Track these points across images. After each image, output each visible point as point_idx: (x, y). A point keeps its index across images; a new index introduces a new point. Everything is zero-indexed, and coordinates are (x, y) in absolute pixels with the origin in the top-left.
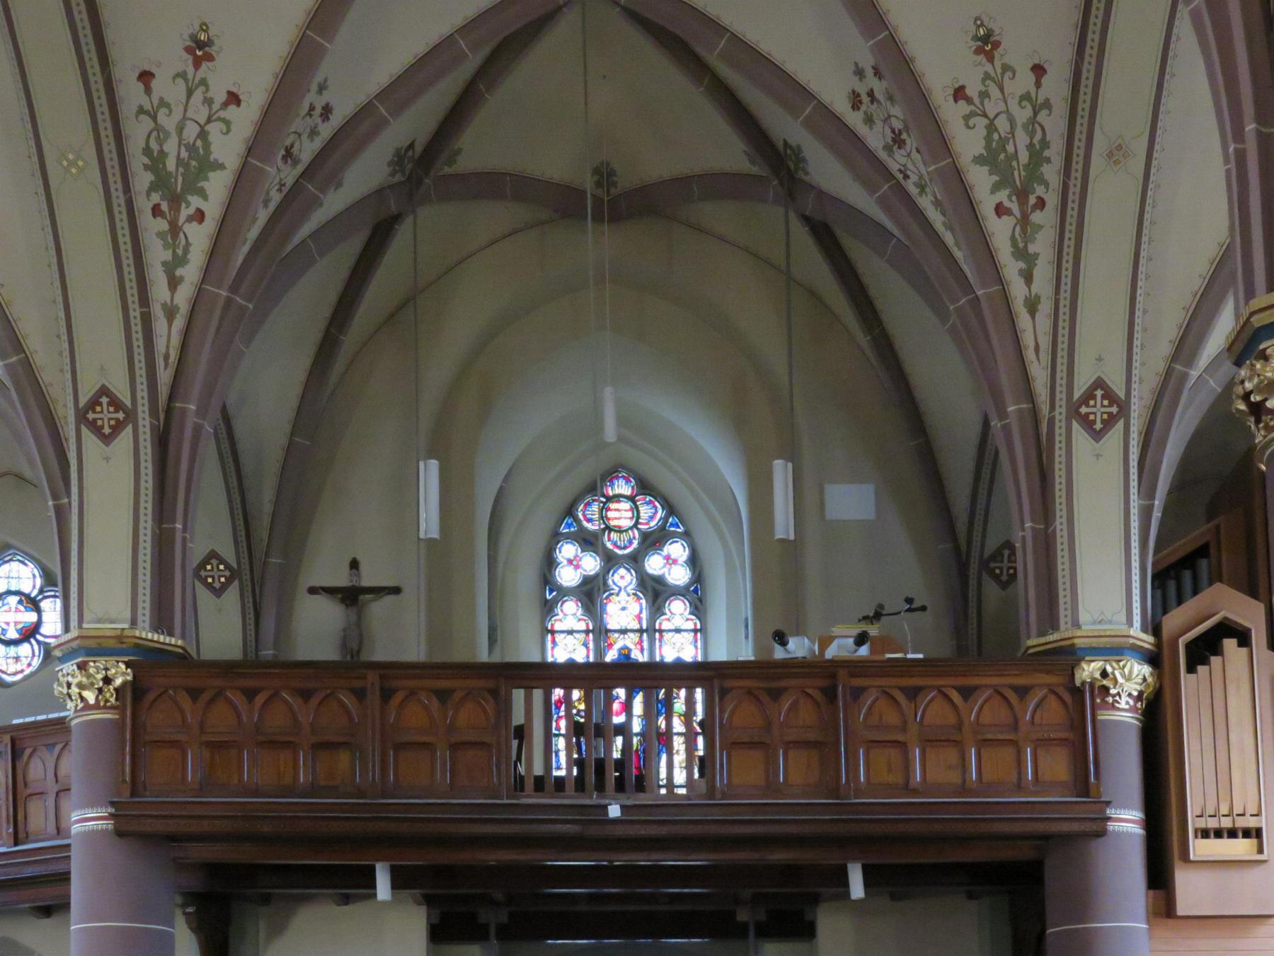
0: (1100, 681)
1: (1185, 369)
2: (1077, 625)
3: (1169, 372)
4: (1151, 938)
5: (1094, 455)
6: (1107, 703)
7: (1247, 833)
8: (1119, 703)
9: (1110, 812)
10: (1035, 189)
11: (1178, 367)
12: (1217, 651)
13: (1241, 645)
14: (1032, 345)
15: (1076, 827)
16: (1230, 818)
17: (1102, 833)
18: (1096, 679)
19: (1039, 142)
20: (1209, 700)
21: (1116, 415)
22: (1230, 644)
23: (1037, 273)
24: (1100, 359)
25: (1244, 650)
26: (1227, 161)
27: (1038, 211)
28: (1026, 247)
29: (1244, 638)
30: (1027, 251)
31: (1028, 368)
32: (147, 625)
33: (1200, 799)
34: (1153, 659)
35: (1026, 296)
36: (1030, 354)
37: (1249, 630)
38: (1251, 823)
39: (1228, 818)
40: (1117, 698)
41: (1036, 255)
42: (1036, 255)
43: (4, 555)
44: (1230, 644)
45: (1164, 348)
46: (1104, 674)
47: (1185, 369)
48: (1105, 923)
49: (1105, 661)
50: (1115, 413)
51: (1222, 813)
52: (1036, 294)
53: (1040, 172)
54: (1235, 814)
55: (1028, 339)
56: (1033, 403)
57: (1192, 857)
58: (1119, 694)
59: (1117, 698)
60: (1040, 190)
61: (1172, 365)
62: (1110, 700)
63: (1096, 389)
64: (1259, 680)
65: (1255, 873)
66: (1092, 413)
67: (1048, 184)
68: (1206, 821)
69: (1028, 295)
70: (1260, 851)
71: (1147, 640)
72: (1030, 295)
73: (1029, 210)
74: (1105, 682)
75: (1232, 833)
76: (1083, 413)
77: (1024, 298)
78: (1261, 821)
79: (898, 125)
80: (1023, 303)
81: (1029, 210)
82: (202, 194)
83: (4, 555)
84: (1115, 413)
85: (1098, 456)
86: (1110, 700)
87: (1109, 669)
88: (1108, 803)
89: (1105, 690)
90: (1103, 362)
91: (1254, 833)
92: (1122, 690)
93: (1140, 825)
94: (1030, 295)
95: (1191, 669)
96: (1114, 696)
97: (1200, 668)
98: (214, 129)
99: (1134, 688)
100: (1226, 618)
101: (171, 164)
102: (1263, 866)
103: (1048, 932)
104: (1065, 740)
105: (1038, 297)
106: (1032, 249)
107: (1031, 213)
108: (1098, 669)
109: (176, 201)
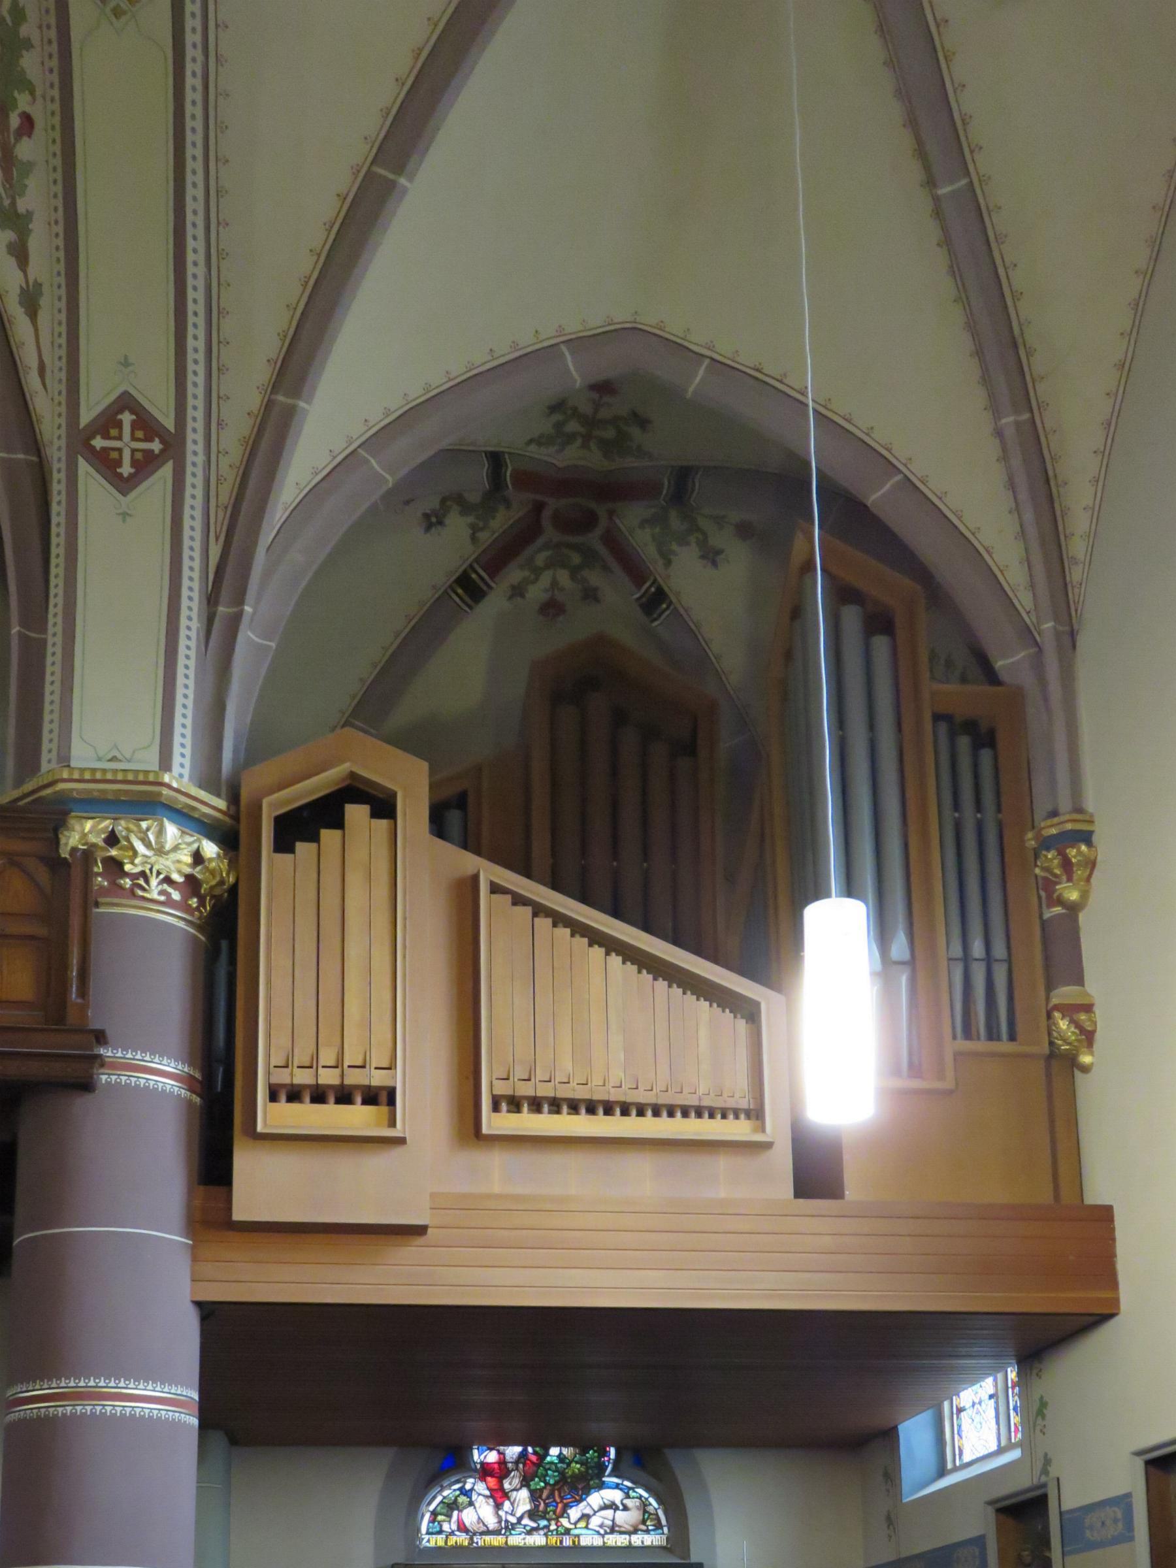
0: (102, 849)
1: (290, 401)
2: (64, 759)
3: (269, 405)
4: (195, 1259)
5: (119, 514)
6: (121, 887)
7: (371, 1097)
8: (144, 889)
9: (106, 1052)
10: (15, 99)
11: (280, 398)
12: (338, 823)
13: (375, 814)
14: (34, 364)
15: (34, 1070)
16: (337, 1071)
17: (86, 1086)
18: (94, 845)
19: (10, 12)
20: (312, 895)
21: (158, 456)
22: (356, 813)
23: (35, 244)
24: (126, 363)
25: (383, 824)
27: (25, 139)
28: (13, 204)
29: (383, 807)
30: (16, 211)
31: (30, 402)
33: (282, 1040)
34: (228, 839)
35: (21, 287)
36: (32, 381)
37: (393, 795)
38: (378, 1079)
39: (337, 1069)
40: (141, 882)
41: (29, 215)
42: (29, 215)
43: (124, 1073)
44: (356, 813)
45: (262, 374)
46: (112, 839)
47: (290, 401)
48: (63, 1228)
49: (115, 819)
50: (157, 452)
51: (322, 1062)
52: (36, 281)
53: (19, 69)
54: (346, 1064)
55: (28, 358)
56: (39, 456)
57: (260, 1128)
58: (143, 874)
59: (141, 882)
60: (23, 101)
61: (273, 397)
62: (127, 883)
63: (121, 411)
64: (405, 869)
65: (377, 1163)
66: (114, 449)
67: (34, 86)
68: (292, 1075)
69: (24, 285)
70: (392, 1123)
71: (214, 804)
72: (27, 282)
73: (12, 140)
74: (114, 852)
75: (344, 1096)
76: (98, 449)
77: (18, 291)
78: (395, 1077)
80: (17, 299)
81: (12, 140)
83: (124, 1073)
84: (157, 452)
85: (125, 515)
86: (127, 883)
87: (121, 829)
88: (100, 1037)
89: (115, 867)
90: (131, 368)
91: (383, 1097)
92: (151, 870)
93: (185, 1085)
94: (27, 282)
95: (284, 844)
96: (134, 877)
97: (300, 846)
99: (178, 864)
100: (352, 775)
102: (397, 1152)
103: (16, 1242)
104: (32, 937)
105: (38, 285)
106: (22, 206)
107: (15, 143)
108: (103, 831)
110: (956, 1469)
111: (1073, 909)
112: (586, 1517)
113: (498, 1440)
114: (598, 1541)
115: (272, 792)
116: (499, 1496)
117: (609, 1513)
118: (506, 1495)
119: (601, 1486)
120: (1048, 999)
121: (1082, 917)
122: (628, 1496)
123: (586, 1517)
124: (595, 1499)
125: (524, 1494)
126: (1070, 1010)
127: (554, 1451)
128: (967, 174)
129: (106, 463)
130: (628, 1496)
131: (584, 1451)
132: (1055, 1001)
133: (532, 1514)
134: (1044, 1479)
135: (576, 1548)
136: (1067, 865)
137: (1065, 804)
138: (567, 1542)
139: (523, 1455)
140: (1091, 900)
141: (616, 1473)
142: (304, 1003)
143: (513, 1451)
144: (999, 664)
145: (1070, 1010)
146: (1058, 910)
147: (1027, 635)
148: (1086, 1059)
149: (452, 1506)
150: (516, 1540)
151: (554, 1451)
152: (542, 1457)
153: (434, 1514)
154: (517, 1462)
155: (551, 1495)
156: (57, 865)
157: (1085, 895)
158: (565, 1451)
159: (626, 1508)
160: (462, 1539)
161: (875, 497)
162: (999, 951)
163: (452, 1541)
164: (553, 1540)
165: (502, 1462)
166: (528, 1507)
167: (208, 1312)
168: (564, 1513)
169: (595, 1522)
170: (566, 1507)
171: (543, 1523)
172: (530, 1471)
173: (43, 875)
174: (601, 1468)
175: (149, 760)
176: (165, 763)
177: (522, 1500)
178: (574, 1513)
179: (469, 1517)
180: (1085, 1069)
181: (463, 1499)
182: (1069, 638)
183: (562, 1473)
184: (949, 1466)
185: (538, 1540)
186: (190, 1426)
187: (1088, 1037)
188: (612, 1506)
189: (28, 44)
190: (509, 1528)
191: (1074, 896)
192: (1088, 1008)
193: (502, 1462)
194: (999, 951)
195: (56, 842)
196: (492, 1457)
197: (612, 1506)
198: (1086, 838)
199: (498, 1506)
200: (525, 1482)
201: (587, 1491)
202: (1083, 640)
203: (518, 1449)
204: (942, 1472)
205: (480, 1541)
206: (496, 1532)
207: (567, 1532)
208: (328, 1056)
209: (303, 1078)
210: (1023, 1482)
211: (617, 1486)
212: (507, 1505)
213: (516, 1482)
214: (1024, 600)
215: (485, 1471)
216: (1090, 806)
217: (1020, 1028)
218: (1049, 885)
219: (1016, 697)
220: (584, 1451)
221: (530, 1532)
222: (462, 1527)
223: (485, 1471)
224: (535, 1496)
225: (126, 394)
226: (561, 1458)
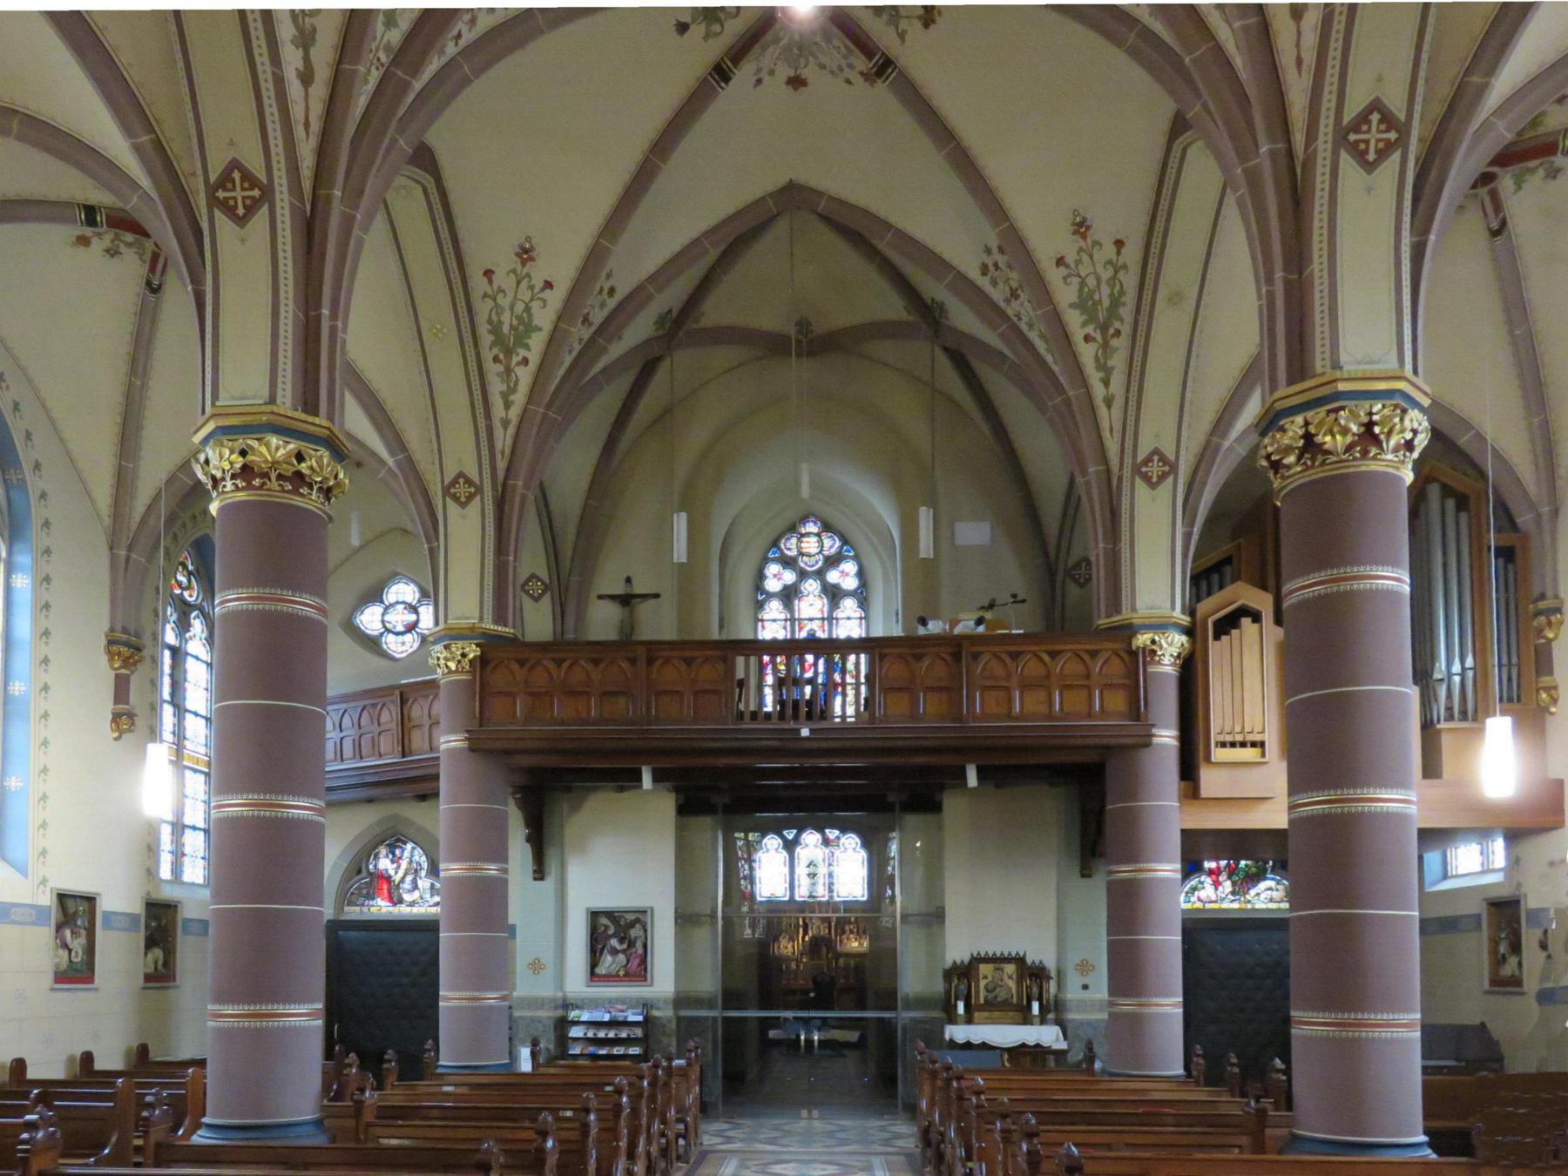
2: (1134, 609)
3: (1208, 442)
9: (1154, 731)
15: (1129, 741)
16: (1241, 735)
17: (1148, 745)
26: (1260, 298)
28: (1105, 363)
29: (1256, 617)
32: (288, 401)
34: (1189, 632)
36: (1106, 434)
38: (1257, 738)
44: (1246, 622)
46: (1153, 642)
55: (1105, 424)
60: (1117, 325)
70: (1263, 755)
74: (1154, 647)
75: (1243, 744)
79: (1014, 285)
82: (528, 348)
89: (1154, 652)
95: (1217, 637)
98: (535, 305)
101: (506, 329)
104: (1124, 685)
106: (1110, 363)
109: (509, 352)
110: (1453, 877)
111: (1550, 641)
112: (1258, 894)
113: (1217, 859)
114: (1263, 906)
115: (1210, 616)
116: (1216, 884)
117: (1269, 892)
118: (1220, 884)
119: (1265, 879)
120: (1537, 684)
121: (1554, 644)
122: (1278, 884)
123: (1258, 894)
124: (1263, 885)
125: (1228, 883)
126: (1548, 689)
127: (1243, 863)
128: (1488, 118)
129: (1146, 478)
130: (1278, 884)
131: (1257, 862)
132: (1541, 685)
133: (1233, 893)
134: (1517, 893)
135: (1254, 910)
136: (1550, 624)
137: (1549, 594)
138: (1249, 906)
139: (1228, 865)
140: (1560, 636)
141: (1273, 871)
142: (1228, 711)
143: (1223, 863)
144: (1519, 521)
145: (1548, 689)
146: (1543, 641)
147: (1532, 506)
148: (1553, 709)
149: (1194, 889)
150: (1225, 905)
151: (1243, 863)
152: (1237, 864)
153: (1187, 893)
154: (1225, 868)
155: (1242, 884)
156: (1133, 654)
157: (1556, 637)
158: (1248, 862)
159: (1277, 890)
160: (1199, 905)
161: (1463, 441)
162: (1514, 660)
163: (1195, 906)
164: (1243, 906)
165: (1218, 868)
166: (1230, 889)
167: (1184, 832)
168: (1247, 892)
169: (1263, 896)
170: (1249, 889)
171: (1238, 897)
172: (1232, 872)
173: (1126, 657)
174: (1265, 871)
175: (1167, 612)
176: (1173, 608)
177: (1227, 886)
178: (1253, 892)
179: (1202, 894)
180: (1552, 714)
181: (1200, 886)
182: (1556, 512)
183: (1247, 873)
184: (1449, 874)
185: (1236, 906)
186: (1177, 879)
187: (1555, 701)
188: (1270, 889)
189: (1124, 304)
190: (1222, 900)
191: (1551, 635)
192: (1555, 688)
193: (1218, 868)
194: (1514, 660)
195: (1130, 643)
196: (1213, 865)
197: (1270, 889)
198: (1558, 610)
199: (1216, 889)
200: (1229, 877)
201: (1258, 882)
202: (1561, 517)
203: (1226, 862)
204: (1445, 877)
205: (1208, 906)
206: (1215, 902)
207: (1249, 902)
208: (1238, 729)
209: (1229, 738)
210: (1505, 893)
211: (1273, 879)
212: (1220, 888)
213: (1225, 877)
214: (1532, 489)
215: (1211, 872)
216: (1562, 595)
217: (1523, 698)
218: (1540, 632)
219: (1526, 538)
220: (1257, 862)
221: (1232, 901)
222: (1199, 899)
223: (1211, 872)
224: (1234, 884)
225: (1156, 448)
226: (1246, 866)
